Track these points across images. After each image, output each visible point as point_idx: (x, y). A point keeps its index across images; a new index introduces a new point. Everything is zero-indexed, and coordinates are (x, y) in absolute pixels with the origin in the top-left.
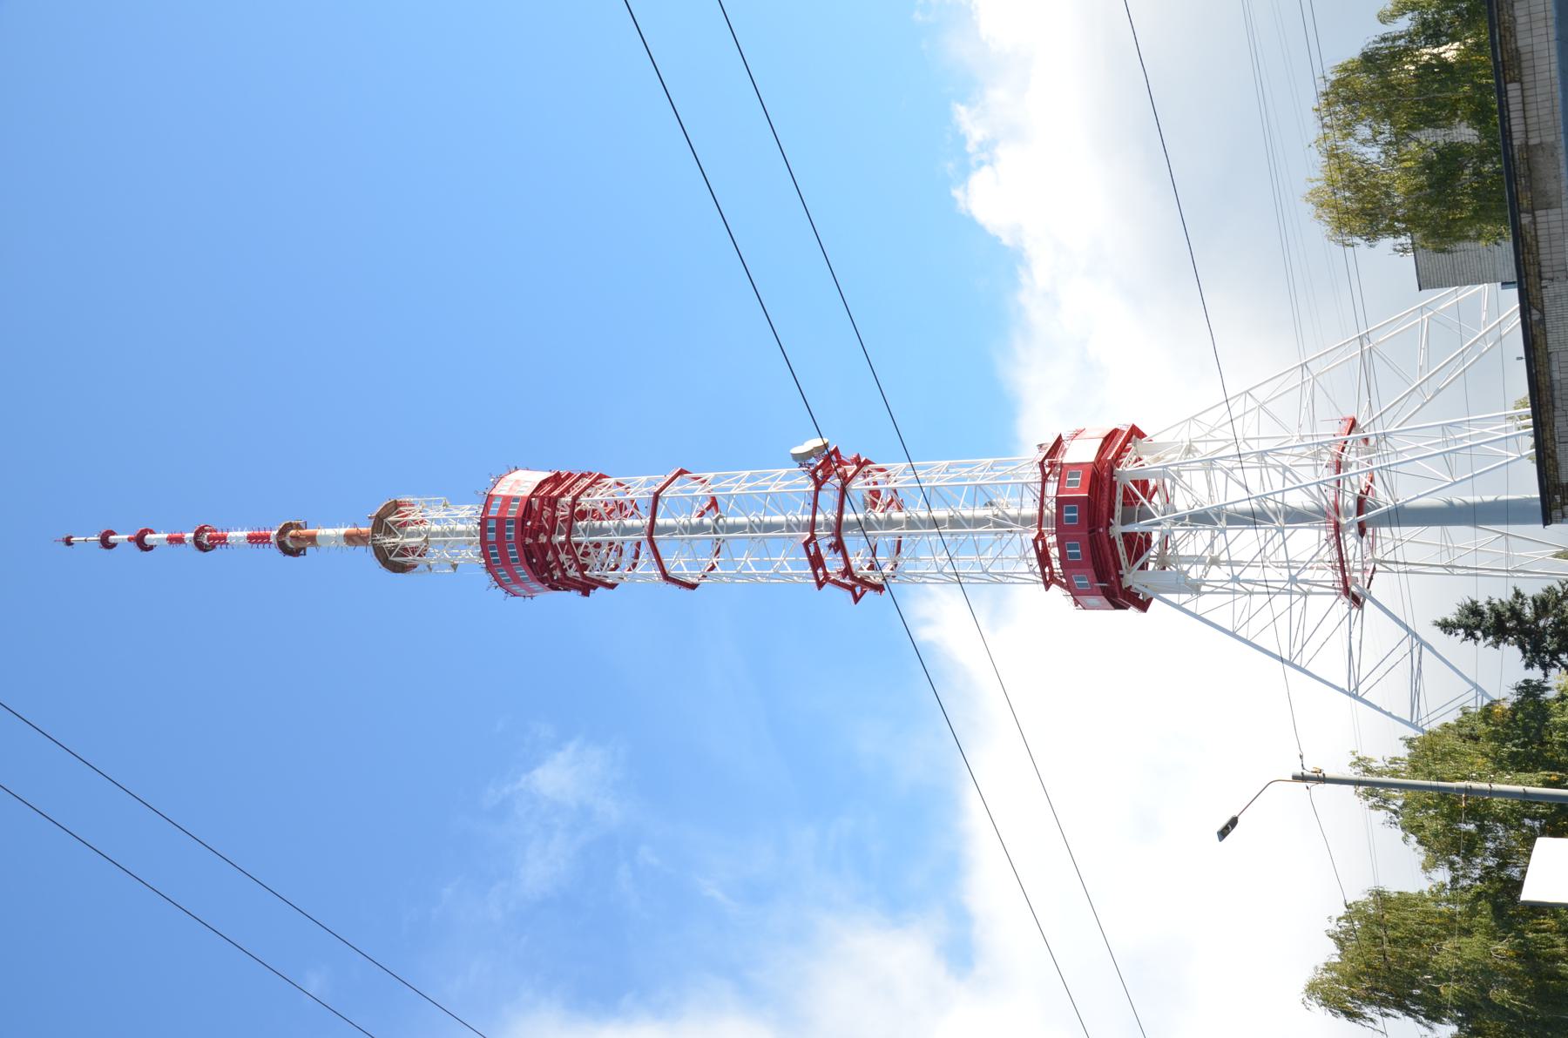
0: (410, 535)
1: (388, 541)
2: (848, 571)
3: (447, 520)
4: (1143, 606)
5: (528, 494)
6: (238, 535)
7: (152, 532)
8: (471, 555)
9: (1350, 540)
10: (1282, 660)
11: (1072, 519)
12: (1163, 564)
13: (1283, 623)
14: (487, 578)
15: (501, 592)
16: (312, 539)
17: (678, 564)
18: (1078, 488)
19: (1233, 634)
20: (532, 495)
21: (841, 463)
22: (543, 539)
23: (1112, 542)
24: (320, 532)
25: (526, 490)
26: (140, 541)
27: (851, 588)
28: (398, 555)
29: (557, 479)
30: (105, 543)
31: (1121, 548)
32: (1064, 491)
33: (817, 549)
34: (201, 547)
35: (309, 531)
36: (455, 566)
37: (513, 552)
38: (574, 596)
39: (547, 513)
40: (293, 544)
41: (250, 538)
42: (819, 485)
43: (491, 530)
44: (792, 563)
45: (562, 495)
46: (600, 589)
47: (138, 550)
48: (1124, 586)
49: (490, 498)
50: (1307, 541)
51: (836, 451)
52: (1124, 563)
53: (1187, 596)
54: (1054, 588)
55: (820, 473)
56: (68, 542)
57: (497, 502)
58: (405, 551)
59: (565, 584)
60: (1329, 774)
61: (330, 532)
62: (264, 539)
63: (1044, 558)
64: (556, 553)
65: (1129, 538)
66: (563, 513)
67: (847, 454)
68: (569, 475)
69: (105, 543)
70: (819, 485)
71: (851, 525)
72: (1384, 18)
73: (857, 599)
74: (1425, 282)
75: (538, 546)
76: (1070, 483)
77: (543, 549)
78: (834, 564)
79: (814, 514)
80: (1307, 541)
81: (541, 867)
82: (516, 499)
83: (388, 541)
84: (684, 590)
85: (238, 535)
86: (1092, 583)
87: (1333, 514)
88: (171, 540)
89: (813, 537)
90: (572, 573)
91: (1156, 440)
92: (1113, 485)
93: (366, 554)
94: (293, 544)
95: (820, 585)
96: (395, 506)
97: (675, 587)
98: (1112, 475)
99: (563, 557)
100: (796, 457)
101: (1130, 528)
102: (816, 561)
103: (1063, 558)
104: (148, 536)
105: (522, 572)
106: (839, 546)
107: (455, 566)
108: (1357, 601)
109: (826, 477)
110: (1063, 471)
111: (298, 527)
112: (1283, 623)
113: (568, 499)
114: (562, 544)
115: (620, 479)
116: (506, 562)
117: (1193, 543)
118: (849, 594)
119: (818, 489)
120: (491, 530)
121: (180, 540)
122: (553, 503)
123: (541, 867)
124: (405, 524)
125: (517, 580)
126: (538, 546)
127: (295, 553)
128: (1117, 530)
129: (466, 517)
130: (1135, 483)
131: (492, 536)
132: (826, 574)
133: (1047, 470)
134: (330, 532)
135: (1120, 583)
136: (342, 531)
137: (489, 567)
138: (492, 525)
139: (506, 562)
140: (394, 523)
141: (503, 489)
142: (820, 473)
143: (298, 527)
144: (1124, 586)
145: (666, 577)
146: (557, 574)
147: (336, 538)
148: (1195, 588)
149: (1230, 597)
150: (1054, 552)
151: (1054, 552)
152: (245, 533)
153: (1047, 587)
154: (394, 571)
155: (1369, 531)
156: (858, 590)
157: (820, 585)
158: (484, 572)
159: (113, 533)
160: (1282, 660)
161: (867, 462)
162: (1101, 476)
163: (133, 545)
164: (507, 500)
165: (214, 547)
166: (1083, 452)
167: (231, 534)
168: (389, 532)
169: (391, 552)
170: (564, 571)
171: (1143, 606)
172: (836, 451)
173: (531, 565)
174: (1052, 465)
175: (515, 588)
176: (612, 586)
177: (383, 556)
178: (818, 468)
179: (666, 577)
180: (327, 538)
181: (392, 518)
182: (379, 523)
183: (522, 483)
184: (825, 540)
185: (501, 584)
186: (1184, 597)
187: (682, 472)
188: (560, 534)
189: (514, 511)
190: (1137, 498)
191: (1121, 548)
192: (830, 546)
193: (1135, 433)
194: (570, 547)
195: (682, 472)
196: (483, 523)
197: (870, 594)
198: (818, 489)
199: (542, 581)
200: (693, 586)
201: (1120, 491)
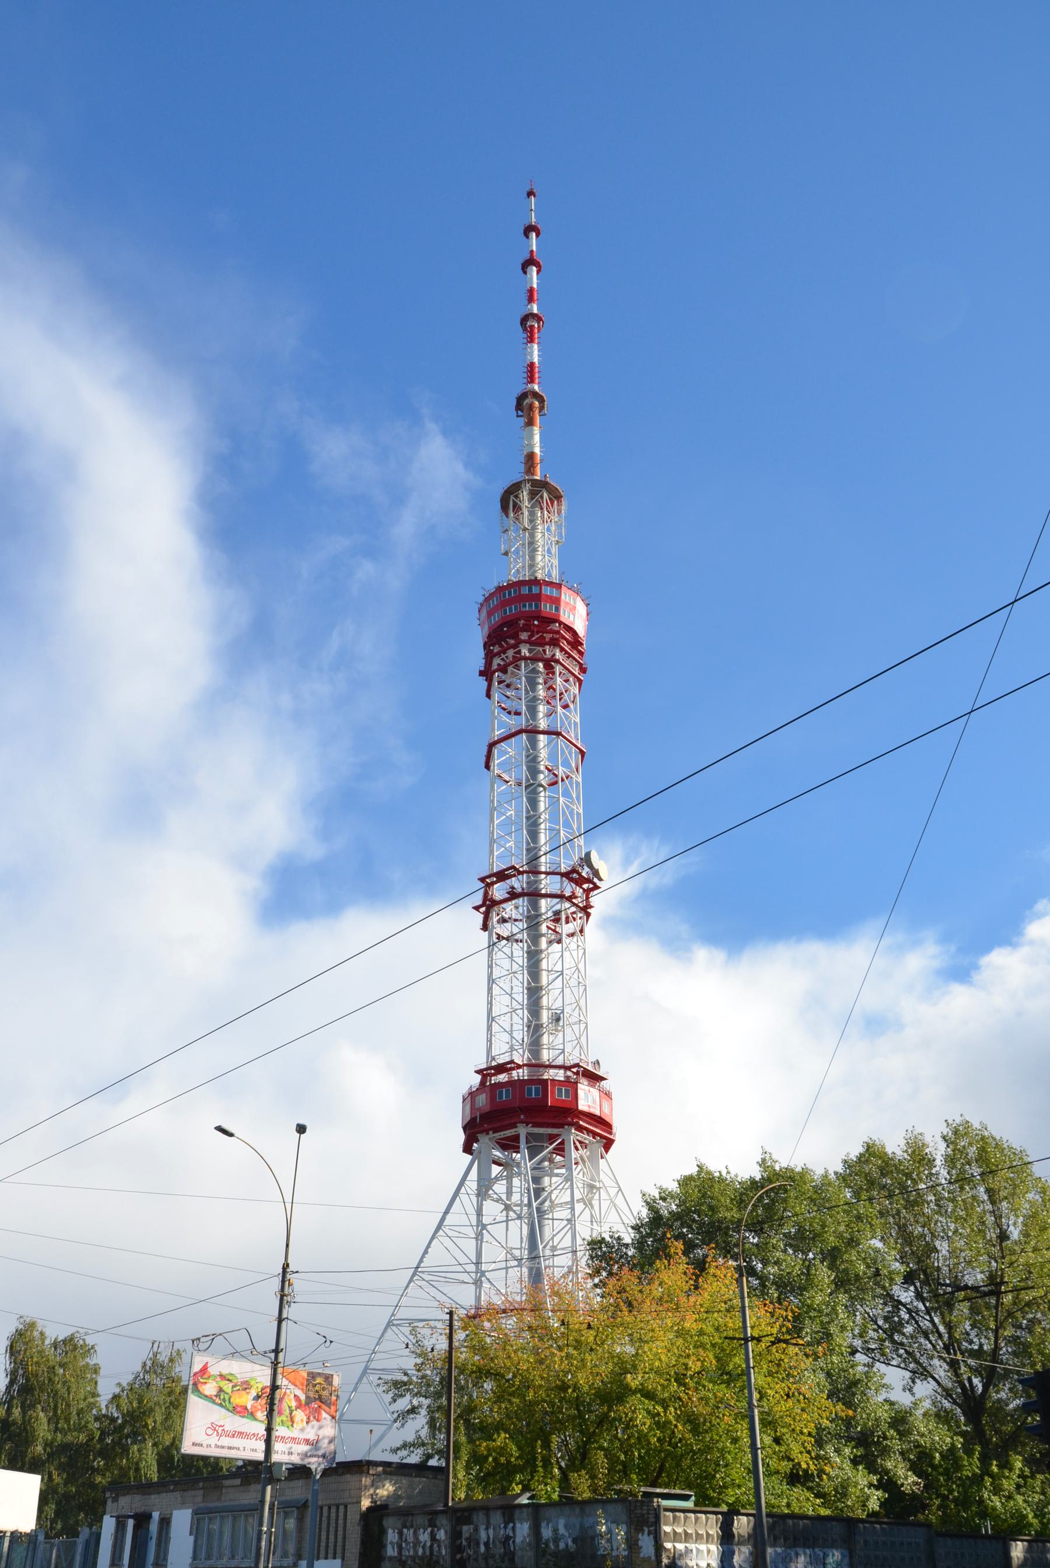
0: (532, 514)
1: (525, 495)
2: (495, 903)
3: (544, 548)
5: (562, 619)
6: (535, 354)
7: (538, 272)
8: (515, 571)
10: (417, 1268)
11: (530, 1093)
13: (459, 1268)
14: (491, 587)
15: (481, 599)
16: (530, 423)
17: (510, 752)
18: (556, 1097)
19: (439, 1227)
20: (561, 623)
24: (536, 430)
25: (565, 617)
26: (530, 262)
28: (514, 502)
29: (576, 642)
30: (529, 229)
31: (508, 1133)
32: (553, 1086)
33: (509, 877)
34: (524, 320)
35: (537, 419)
36: (506, 554)
37: (512, 610)
38: (480, 663)
39: (548, 636)
40: (526, 405)
41: (532, 365)
42: (566, 875)
43: (530, 590)
44: (508, 852)
45: (562, 650)
46: (486, 683)
47: (521, 261)
48: (479, 1136)
49: (559, 586)
51: (596, 887)
54: (479, 1077)
55: (575, 875)
56: (530, 194)
58: (517, 508)
59: (489, 656)
61: (537, 438)
63: (501, 1068)
64: (515, 646)
65: (516, 1138)
66: (549, 651)
68: (581, 653)
69: (529, 229)
70: (566, 875)
71: (535, 906)
73: (477, 908)
75: (520, 628)
76: (560, 1091)
77: (515, 636)
78: (499, 891)
79: (547, 873)
81: (336, 452)
82: (557, 609)
83: (525, 495)
84: (484, 759)
85: (535, 354)
86: (479, 1109)
88: (531, 291)
91: (602, 1162)
92: (561, 1126)
93: (516, 472)
94: (526, 405)
95: (482, 880)
96: (556, 496)
100: (588, 855)
102: (502, 876)
103: (500, 1085)
104: (534, 269)
105: (496, 618)
106: (513, 895)
107: (506, 554)
109: (571, 880)
110: (571, 1086)
111: (541, 408)
112: (459, 1268)
113: (558, 655)
114: (519, 652)
116: (504, 604)
118: (480, 902)
119: (562, 875)
120: (530, 590)
121: (531, 300)
122: (554, 643)
123: (336, 452)
125: (490, 614)
126: (520, 628)
127: (519, 406)
128: (522, 1131)
129: (547, 564)
130: (562, 1143)
131: (525, 590)
132: (493, 883)
133: (574, 1070)
134: (537, 438)
135: (481, 1132)
136: (537, 450)
137: (500, 589)
138: (535, 590)
139: (504, 604)
140: (542, 497)
141: (566, 596)
142: (575, 875)
143: (541, 408)
144: (479, 1136)
145: (492, 746)
146: (496, 649)
147: (532, 446)
148: (507, 516)
149: (474, 1223)
150: (502, 1078)
151: (502, 1078)
152: (536, 360)
154: (501, 501)
157: (482, 880)
158: (496, 584)
159: (537, 236)
160: (417, 1268)
161: (588, 915)
162: (567, 1115)
163: (527, 256)
164: (556, 601)
165: (525, 330)
166: (587, 1099)
167: (536, 346)
168: (533, 494)
169: (517, 497)
170: (498, 654)
172: (596, 887)
173: (502, 626)
174: (577, 1073)
175: (495, 601)
178: (579, 874)
180: (531, 436)
181: (545, 495)
183: (575, 614)
184: (518, 883)
185: (487, 600)
186: (474, 1186)
187: (582, 753)
188: (530, 651)
189: (547, 608)
190: (551, 1144)
191: (508, 1133)
192: (513, 888)
194: (518, 658)
195: (582, 753)
196: (536, 582)
197: (479, 918)
198: (562, 875)
199: (489, 637)
200: (487, 767)
201: (555, 1131)
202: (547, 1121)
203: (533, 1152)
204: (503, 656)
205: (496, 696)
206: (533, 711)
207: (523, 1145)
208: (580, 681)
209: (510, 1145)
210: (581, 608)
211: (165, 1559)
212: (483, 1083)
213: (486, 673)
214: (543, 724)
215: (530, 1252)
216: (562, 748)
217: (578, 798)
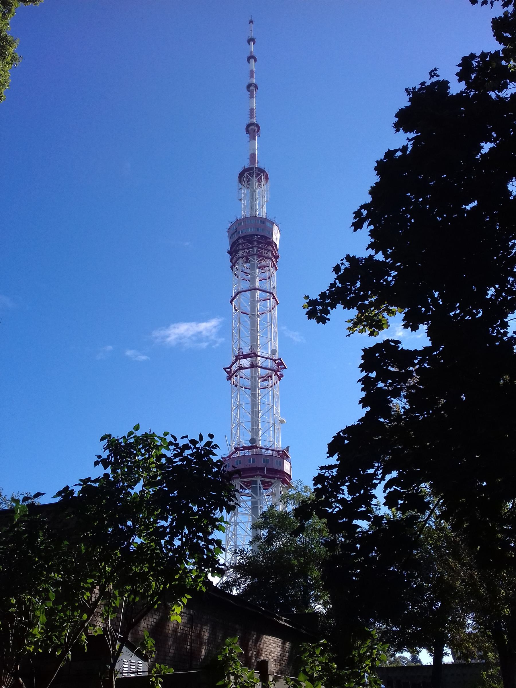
26: (251, 57)
30: (251, 40)
31: (253, 479)
34: (249, 86)
40: (251, 87)
52: (244, 480)
56: (251, 22)
57: (270, 225)
62: (252, 115)
67: (284, 372)
68: (277, 262)
72: (384, 492)
74: (361, 229)
90: (241, 247)
92: (274, 478)
98: (277, 478)
101: (259, 482)
129: (262, 211)
141: (275, 228)
147: (254, 150)
161: (280, 379)
163: (249, 55)
165: (249, 91)
177: (245, 170)
182: (261, 171)
183: (276, 237)
187: (277, 303)
191: (253, 479)
200: (231, 302)
204: (243, 251)
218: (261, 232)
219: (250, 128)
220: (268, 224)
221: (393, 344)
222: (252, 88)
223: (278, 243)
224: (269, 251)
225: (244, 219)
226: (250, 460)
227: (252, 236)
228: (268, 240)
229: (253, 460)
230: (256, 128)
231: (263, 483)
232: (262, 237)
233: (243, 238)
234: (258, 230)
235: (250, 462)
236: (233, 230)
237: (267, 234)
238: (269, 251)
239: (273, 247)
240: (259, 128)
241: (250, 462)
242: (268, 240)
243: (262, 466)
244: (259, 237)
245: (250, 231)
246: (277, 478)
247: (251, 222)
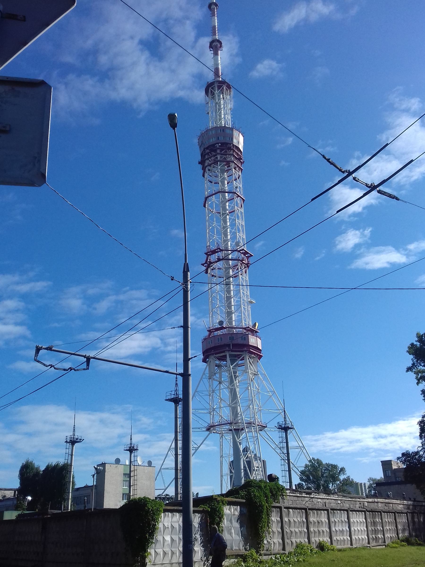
1: (216, 85)
4: (204, 361)
9: (228, 427)
12: (218, 366)
18: (240, 341)
21: (248, 257)
22: (218, 151)
23: (224, 352)
27: (206, 263)
28: (211, 91)
31: (222, 354)
33: (218, 252)
50: (226, 414)
52: (217, 355)
53: (208, 375)
58: (213, 94)
60: (170, 371)
64: (214, 156)
77: (215, 151)
78: (213, 258)
80: (226, 414)
87: (235, 422)
89: (222, 250)
90: (206, 157)
92: (242, 351)
95: (206, 254)
96: (229, 87)
97: (204, 200)
98: (246, 351)
99: (213, 158)
106: (219, 260)
108: (208, 430)
110: (246, 338)
114: (217, 158)
115: (241, 177)
117: (225, 376)
124: (223, 93)
127: (211, 46)
129: (226, 119)
140: (223, 88)
141: (235, 133)
145: (206, 198)
148: (208, 96)
153: (208, 331)
155: (231, 432)
156: (206, 265)
168: (219, 87)
170: (208, 159)
171: (204, 361)
176: (204, 176)
179: (206, 198)
183: (239, 141)
184: (221, 255)
187: (244, 200)
191: (222, 354)
193: (260, 357)
194: (216, 162)
195: (244, 200)
200: (205, 206)
202: (236, 350)
203: (232, 362)
204: (210, 160)
205: (206, 175)
206: (223, 184)
207: (228, 359)
208: (242, 170)
209: (223, 358)
210: (241, 139)
211: (25, 186)
212: (210, 335)
213: (202, 162)
214: (227, 189)
215: (229, 288)
216: (245, 467)
217: (242, 218)
218: (222, 139)
219: (213, 44)
220: (228, 131)
221: (17, 492)
222: (213, 6)
223: (241, 147)
224: (231, 155)
225: (206, 131)
226: (219, 339)
227: (213, 145)
228: (229, 146)
229: (221, 338)
230: (218, 43)
231: (231, 356)
232: (223, 144)
233: (207, 148)
234: (218, 138)
235: (219, 341)
236: (201, 143)
237: (227, 140)
238: (231, 155)
239: (234, 151)
240: (221, 43)
241: (219, 341)
242: (229, 146)
243: (229, 343)
244: (220, 144)
245: (212, 141)
246: (246, 351)
247: (212, 133)
